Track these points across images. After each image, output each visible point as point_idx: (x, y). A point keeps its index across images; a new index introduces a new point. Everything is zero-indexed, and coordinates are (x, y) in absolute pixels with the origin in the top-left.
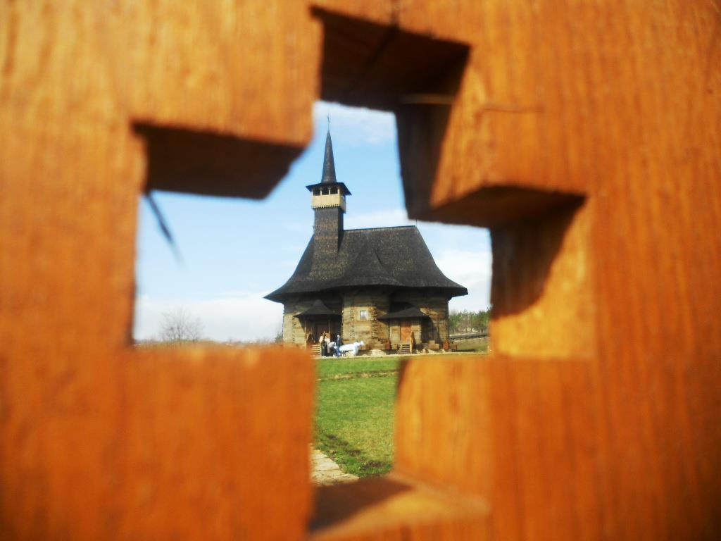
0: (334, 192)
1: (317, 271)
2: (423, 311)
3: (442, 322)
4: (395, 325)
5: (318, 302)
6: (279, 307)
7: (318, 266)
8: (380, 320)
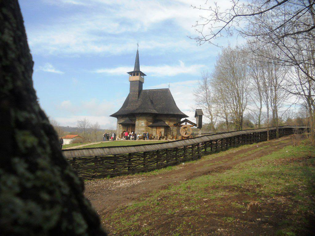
0: (137, 75)
2: (167, 123)
5: (127, 119)
6: (115, 119)
8: (149, 126)
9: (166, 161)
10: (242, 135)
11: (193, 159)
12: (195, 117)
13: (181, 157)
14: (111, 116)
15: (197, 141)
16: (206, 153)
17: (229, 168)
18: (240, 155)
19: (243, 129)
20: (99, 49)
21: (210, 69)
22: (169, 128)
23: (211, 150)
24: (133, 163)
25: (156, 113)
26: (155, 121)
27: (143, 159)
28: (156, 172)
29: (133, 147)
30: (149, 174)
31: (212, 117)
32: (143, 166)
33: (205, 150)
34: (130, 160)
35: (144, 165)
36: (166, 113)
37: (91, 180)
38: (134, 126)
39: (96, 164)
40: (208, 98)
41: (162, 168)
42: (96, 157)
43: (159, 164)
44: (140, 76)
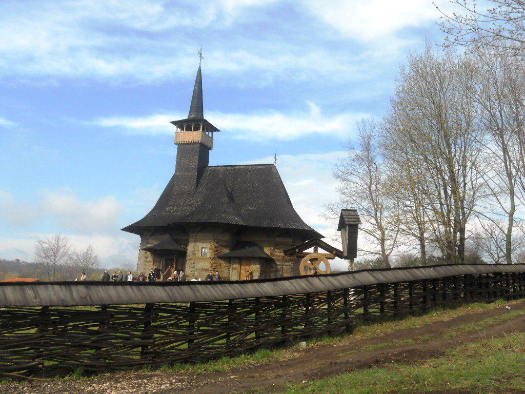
0: (197, 128)
1: (174, 206)
2: (267, 251)
3: (287, 264)
4: (235, 263)
5: (166, 237)
6: (136, 239)
7: (176, 202)
9: (253, 335)
10: (466, 276)
11: (330, 333)
12: (339, 229)
13: (297, 324)
14: (123, 230)
15: (342, 284)
16: (367, 319)
17: (436, 354)
18: (462, 326)
19: (464, 263)
20: (107, 68)
21: (377, 119)
22: (273, 265)
23: (382, 311)
24: (156, 335)
25: (242, 225)
26: (237, 244)
27: (187, 324)
28: (224, 365)
29: (160, 288)
30: (200, 368)
31: (383, 234)
32: (185, 346)
33: (366, 310)
34: (147, 324)
35: (190, 341)
36: (265, 224)
37: (24, 380)
38: (183, 255)
39: (41, 331)
40: (373, 188)
41: (241, 353)
42: (45, 308)
43: (234, 341)
44: (203, 130)
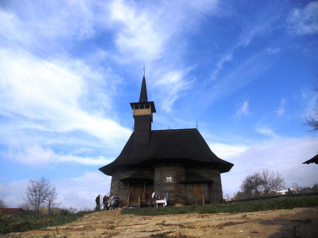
0: (147, 107)
8: (181, 183)
